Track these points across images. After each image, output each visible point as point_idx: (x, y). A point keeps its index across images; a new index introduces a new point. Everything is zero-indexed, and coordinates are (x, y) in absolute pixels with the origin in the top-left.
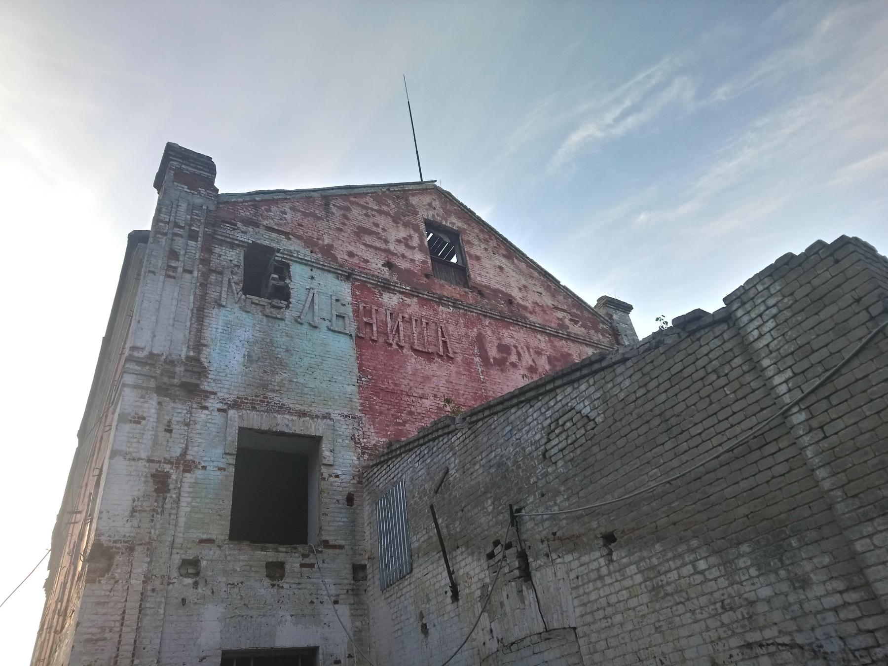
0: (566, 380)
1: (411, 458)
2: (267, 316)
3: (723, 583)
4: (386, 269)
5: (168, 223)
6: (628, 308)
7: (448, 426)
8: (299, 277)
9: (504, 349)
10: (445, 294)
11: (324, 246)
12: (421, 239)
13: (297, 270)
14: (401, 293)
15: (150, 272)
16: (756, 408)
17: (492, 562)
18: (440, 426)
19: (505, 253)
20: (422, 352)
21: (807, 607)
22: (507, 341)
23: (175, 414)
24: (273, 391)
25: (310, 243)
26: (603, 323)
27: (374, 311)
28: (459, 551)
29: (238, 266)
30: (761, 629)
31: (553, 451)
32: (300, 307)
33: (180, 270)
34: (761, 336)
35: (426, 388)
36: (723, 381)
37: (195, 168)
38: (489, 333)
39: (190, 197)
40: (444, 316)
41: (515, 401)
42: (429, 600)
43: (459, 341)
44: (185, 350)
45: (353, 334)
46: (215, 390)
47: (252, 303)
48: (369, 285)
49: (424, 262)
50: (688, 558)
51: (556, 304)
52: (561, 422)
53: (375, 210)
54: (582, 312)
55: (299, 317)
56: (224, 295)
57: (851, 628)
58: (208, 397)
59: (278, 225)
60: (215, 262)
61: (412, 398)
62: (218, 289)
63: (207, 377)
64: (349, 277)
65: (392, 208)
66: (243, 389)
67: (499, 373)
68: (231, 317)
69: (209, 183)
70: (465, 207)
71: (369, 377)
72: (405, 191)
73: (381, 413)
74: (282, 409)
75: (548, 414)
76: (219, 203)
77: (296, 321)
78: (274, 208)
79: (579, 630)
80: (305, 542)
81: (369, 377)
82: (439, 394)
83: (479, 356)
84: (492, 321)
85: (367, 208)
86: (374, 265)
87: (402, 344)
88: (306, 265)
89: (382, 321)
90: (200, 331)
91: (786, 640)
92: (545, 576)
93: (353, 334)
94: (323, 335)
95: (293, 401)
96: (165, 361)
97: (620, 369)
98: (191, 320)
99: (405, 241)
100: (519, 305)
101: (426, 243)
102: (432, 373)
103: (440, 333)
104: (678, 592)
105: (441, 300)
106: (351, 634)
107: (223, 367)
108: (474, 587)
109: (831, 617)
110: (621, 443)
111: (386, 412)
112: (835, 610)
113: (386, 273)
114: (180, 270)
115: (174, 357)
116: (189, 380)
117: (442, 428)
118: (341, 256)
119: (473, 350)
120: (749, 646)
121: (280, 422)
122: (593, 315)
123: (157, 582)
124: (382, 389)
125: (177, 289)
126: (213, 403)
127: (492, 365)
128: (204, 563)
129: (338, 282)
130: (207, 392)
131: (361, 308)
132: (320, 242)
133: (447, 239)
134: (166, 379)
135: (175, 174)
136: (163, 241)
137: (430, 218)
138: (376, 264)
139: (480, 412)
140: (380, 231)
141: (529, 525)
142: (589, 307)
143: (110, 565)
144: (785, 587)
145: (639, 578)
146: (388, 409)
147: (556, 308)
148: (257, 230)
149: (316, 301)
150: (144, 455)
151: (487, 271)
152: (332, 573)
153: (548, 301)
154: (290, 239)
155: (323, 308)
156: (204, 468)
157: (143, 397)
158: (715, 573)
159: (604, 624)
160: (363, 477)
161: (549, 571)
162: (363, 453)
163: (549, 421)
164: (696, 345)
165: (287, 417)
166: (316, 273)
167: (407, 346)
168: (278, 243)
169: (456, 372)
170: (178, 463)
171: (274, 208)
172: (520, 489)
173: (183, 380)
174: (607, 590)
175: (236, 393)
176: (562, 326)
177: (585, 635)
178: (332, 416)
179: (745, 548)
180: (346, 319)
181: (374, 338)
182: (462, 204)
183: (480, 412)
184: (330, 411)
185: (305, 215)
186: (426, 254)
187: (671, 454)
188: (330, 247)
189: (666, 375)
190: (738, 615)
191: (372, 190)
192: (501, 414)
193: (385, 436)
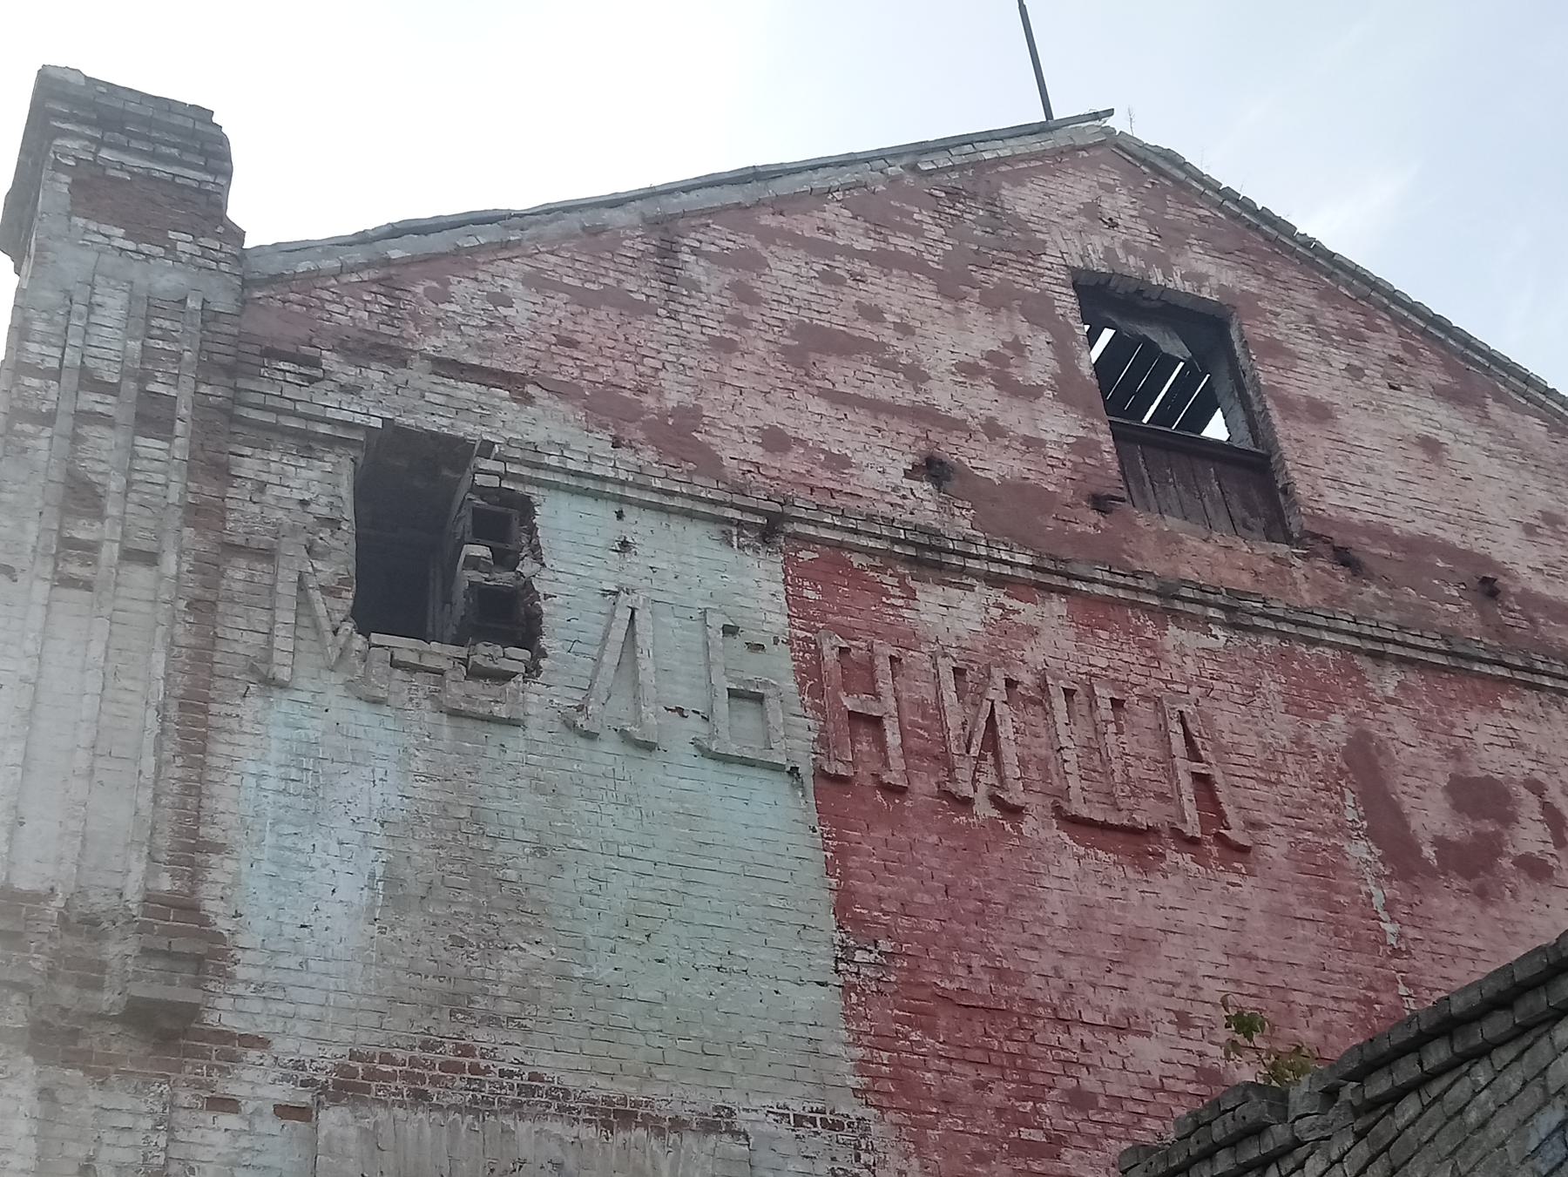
2: (455, 714)
4: (923, 488)
5: (56, 375)
7: (1257, 1130)
8: (573, 551)
9: (1481, 797)
10: (1187, 572)
11: (664, 415)
12: (1063, 350)
14: (994, 581)
18: (1217, 1132)
19: (1441, 378)
20: (1105, 826)
23: (108, 1137)
24: (492, 1020)
25: (610, 409)
27: (883, 665)
29: (333, 523)
32: (584, 666)
33: (110, 552)
35: (1136, 984)
37: (154, 156)
38: (1405, 729)
39: (136, 271)
40: (1191, 668)
43: (1271, 772)
44: (138, 867)
45: (806, 769)
46: (262, 1027)
47: (395, 664)
48: (857, 560)
49: (1083, 447)
53: (863, 255)
55: (580, 709)
56: (283, 641)
58: (234, 1059)
61: (1080, 1033)
62: (260, 617)
63: (231, 978)
64: (770, 530)
65: (932, 238)
66: (373, 1020)
67: (1472, 908)
68: (314, 728)
69: (206, 209)
70: (1247, 205)
71: (885, 945)
72: (979, 165)
73: (947, 1102)
76: (246, 284)
77: (571, 726)
78: (461, 287)
81: (885, 945)
82: (1198, 1012)
83: (1370, 834)
84: (1413, 679)
85: (825, 250)
86: (872, 475)
87: (1015, 796)
88: (597, 496)
89: (921, 705)
93: (806, 769)
94: (679, 777)
95: (576, 1062)
96: (63, 919)
98: (159, 748)
99: (998, 370)
100: (1530, 600)
101: (1087, 371)
102: (1157, 919)
103: (1178, 743)
105: (1171, 602)
107: (290, 931)
111: (970, 1096)
113: (924, 504)
114: (110, 552)
115: (99, 902)
116: (157, 992)
117: (1232, 1143)
118: (737, 451)
119: (1337, 809)
121: (526, 1151)
124: (945, 998)
125: (101, 628)
126: (257, 1084)
127: (1433, 873)
129: (728, 556)
130: (225, 1037)
131: (830, 656)
132: (649, 401)
133: (1173, 346)
134: (67, 994)
135: (75, 185)
136: (42, 444)
137: (1098, 264)
138: (881, 471)
139: (1401, 1052)
140: (888, 335)
146: (980, 1086)
148: (400, 375)
149: (644, 637)
151: (1362, 459)
154: (528, 400)
155: (675, 662)
165: (556, 1127)
166: (639, 525)
167: (1036, 805)
168: (483, 420)
169: (1268, 912)
171: (461, 287)
175: (345, 1035)
178: (742, 1121)
180: (769, 702)
181: (893, 777)
182: (1229, 194)
183: (1401, 1052)
184: (733, 1098)
185: (584, 300)
186: (1089, 411)
188: (690, 417)
191: (848, 177)
192: (1505, 1055)
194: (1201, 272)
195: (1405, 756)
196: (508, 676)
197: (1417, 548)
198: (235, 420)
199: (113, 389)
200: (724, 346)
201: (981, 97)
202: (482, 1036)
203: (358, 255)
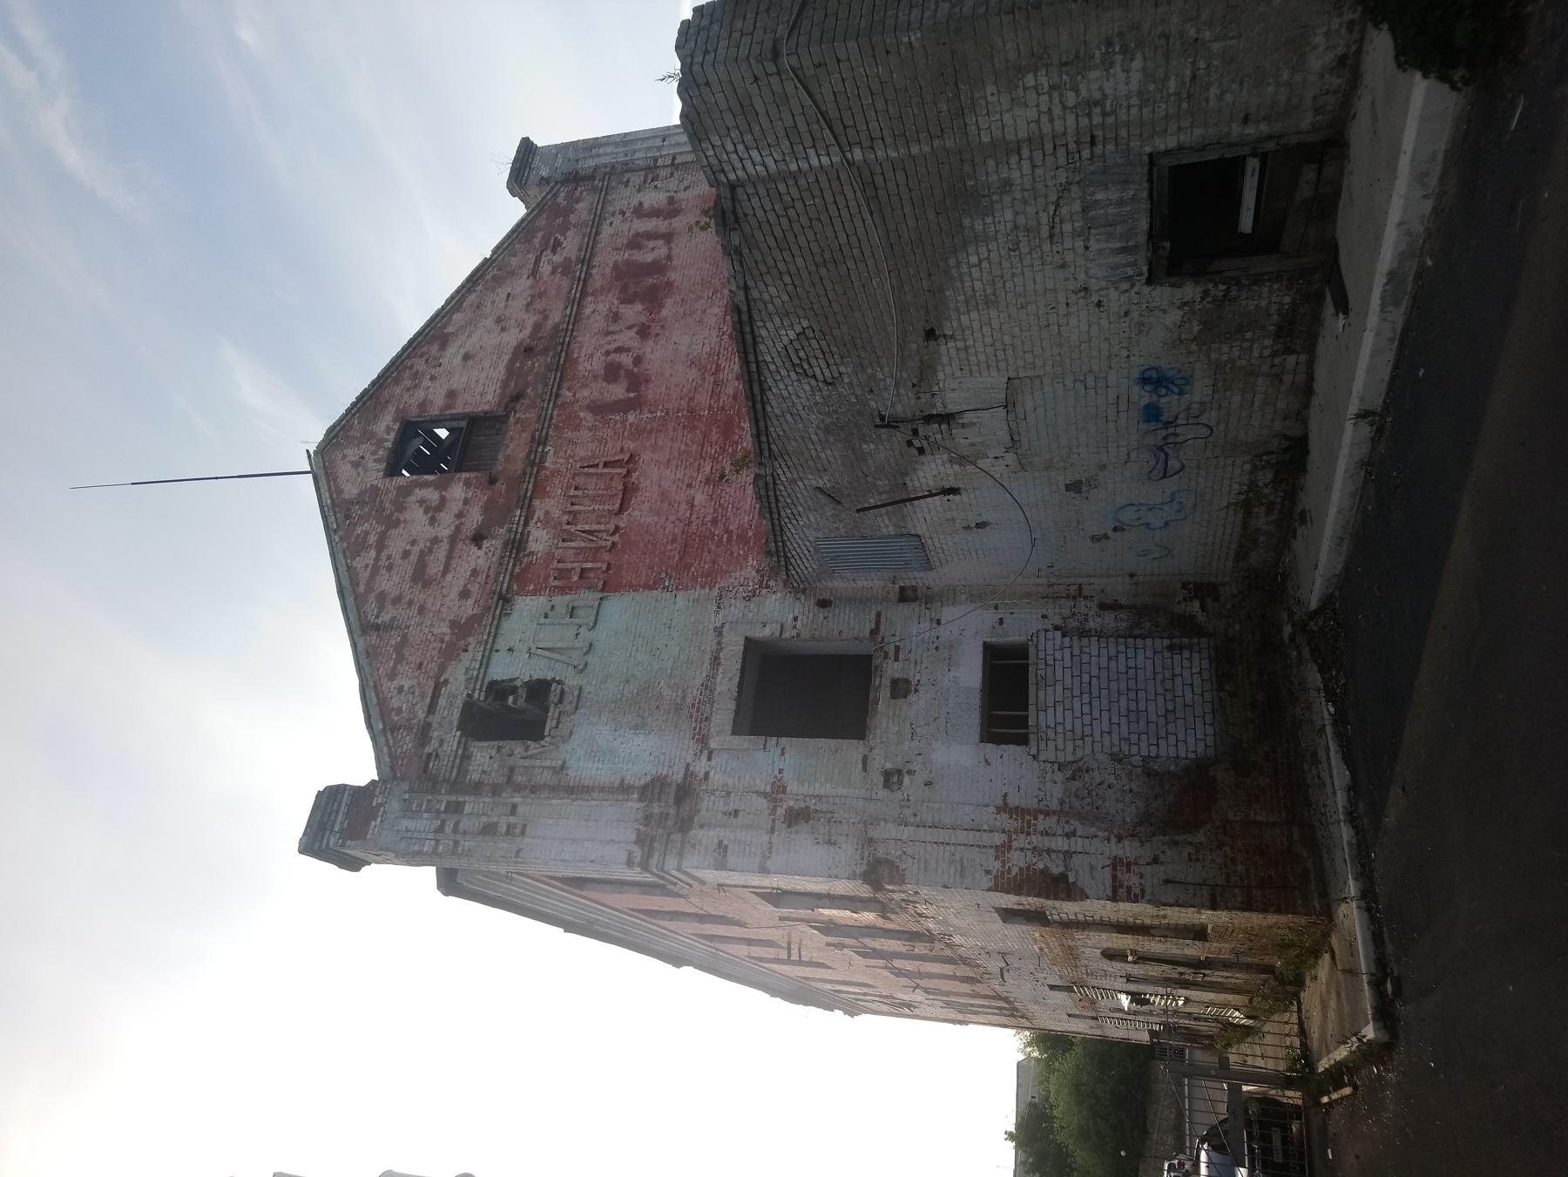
0: (750, 350)
1: (791, 529)
3: (993, 246)
4: (486, 544)
5: (437, 841)
6: (527, 147)
9: (612, 373)
10: (522, 455)
13: (500, 669)
14: (526, 523)
15: (517, 856)
16: (835, 184)
17: (928, 450)
21: (1028, 186)
22: (597, 364)
24: (684, 698)
25: (451, 652)
26: (556, 195)
27: (561, 565)
28: (909, 484)
29: (499, 749)
30: (1039, 224)
31: (827, 374)
33: (512, 820)
34: (764, 165)
36: (799, 205)
37: (337, 812)
38: (586, 393)
41: (759, 406)
42: (953, 519)
43: (602, 441)
48: (517, 570)
49: (468, 484)
50: (965, 269)
51: (526, 272)
52: (796, 361)
53: (378, 554)
54: (539, 230)
56: (548, 763)
57: (1050, 160)
60: (496, 777)
64: (505, 600)
69: (358, 796)
72: (334, 505)
73: (714, 562)
74: (708, 686)
75: (784, 373)
78: (395, 703)
79: (1012, 375)
80: (869, 658)
82: (687, 481)
84: (565, 385)
85: (375, 571)
87: (611, 527)
89: (576, 555)
90: (602, 789)
91: (1052, 208)
92: (953, 400)
93: (599, 595)
97: (755, 294)
99: (433, 512)
100: (532, 336)
102: (655, 488)
103: (591, 470)
104: (993, 283)
105: (535, 462)
106: (973, 606)
108: (950, 471)
109: (1039, 172)
110: (836, 308)
112: (1034, 166)
113: (493, 545)
115: (640, 815)
116: (672, 796)
118: (469, 608)
120: (1051, 236)
122: (541, 211)
123: (907, 811)
124: (681, 559)
126: (701, 767)
128: (889, 766)
129: (515, 615)
130: (685, 776)
131: (557, 583)
132: (447, 638)
134: (670, 823)
140: (416, 549)
141: (899, 408)
142: (527, 215)
143: (887, 861)
144: (1007, 199)
145: (974, 315)
147: (534, 273)
148: (435, 725)
149: (549, 645)
150: (765, 838)
151: (475, 381)
152: (907, 625)
153: (522, 285)
154: (446, 681)
156: (781, 771)
157: (694, 846)
158: (983, 251)
159: (1009, 352)
160: (798, 588)
161: (949, 395)
162: (768, 586)
163: (793, 374)
164: (753, 220)
166: (502, 644)
170: (775, 800)
172: (859, 413)
173: (671, 806)
174: (979, 344)
176: (565, 268)
177: (1017, 370)
178: (718, 624)
179: (966, 222)
185: (400, 658)
186: (452, 479)
187: (861, 265)
188: (454, 624)
189: (776, 252)
190: (1024, 241)
191: (341, 557)
193: (746, 558)
194: (386, 426)
195: (596, 395)
196: (562, 691)
197: (510, 369)
198: (455, 781)
199: (443, 822)
200: (422, 610)
201: (302, 500)
202: (689, 700)
203: (382, 740)
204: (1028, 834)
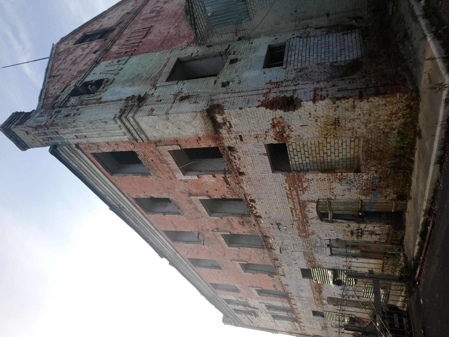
59: (61, 89)
70: (71, 33)
74: (160, 73)
99: (83, 50)
129: (99, 66)
130: (144, 95)
151: (106, 23)
204: (279, 87)
